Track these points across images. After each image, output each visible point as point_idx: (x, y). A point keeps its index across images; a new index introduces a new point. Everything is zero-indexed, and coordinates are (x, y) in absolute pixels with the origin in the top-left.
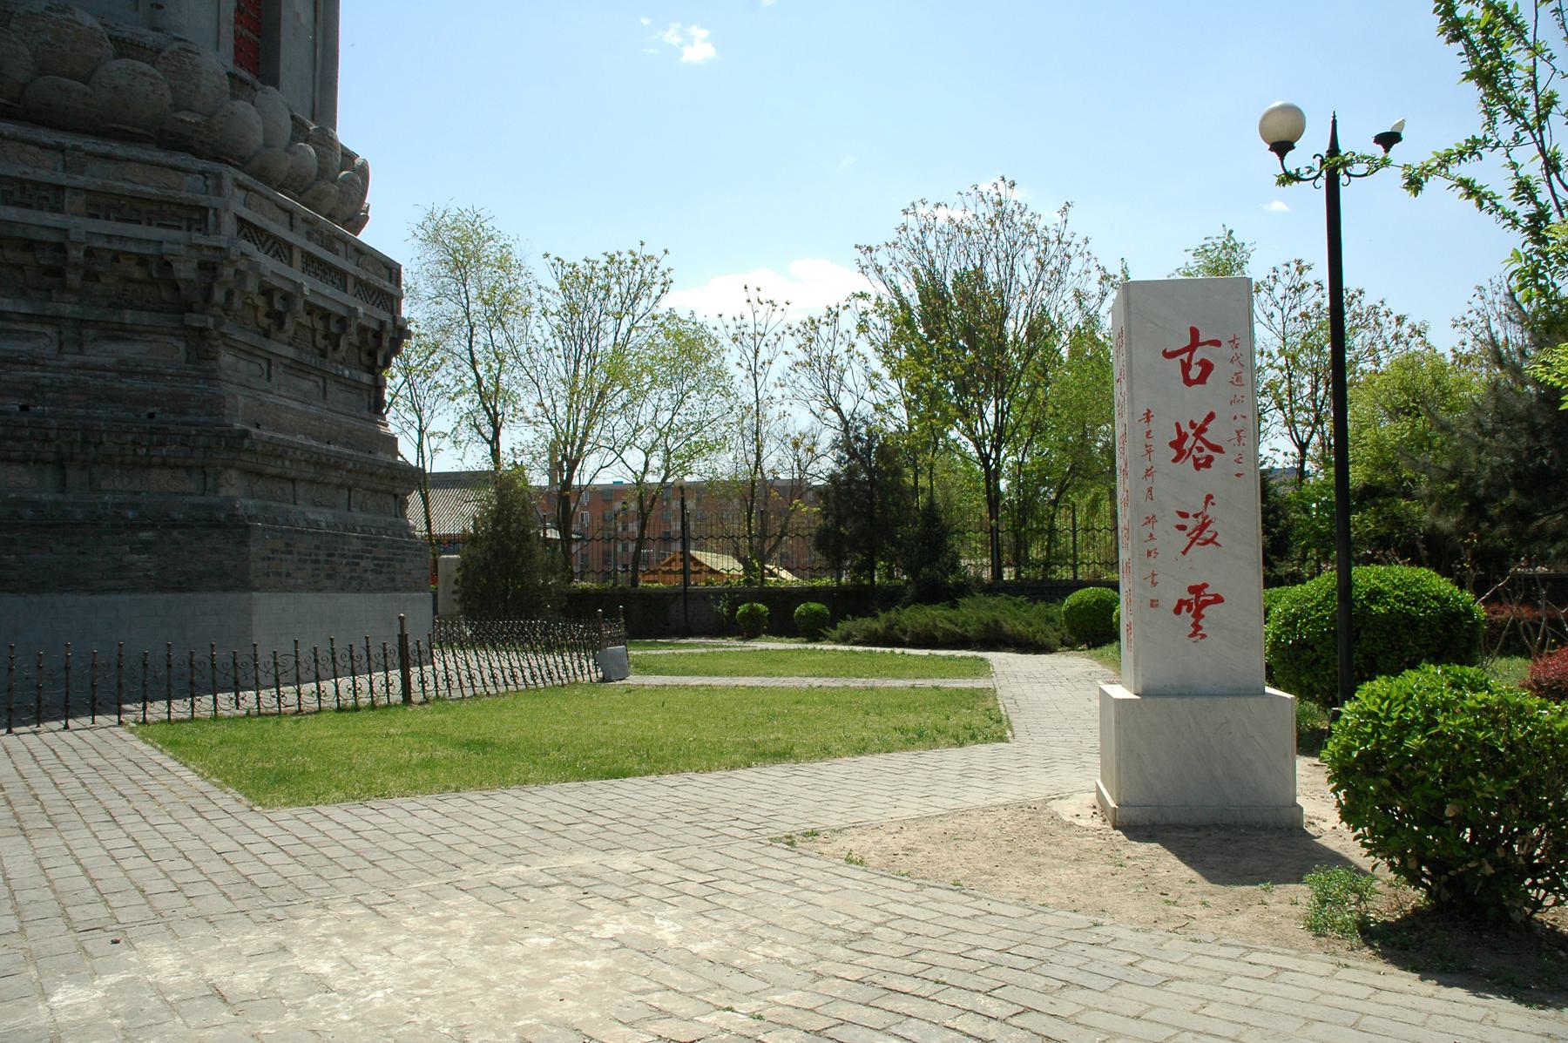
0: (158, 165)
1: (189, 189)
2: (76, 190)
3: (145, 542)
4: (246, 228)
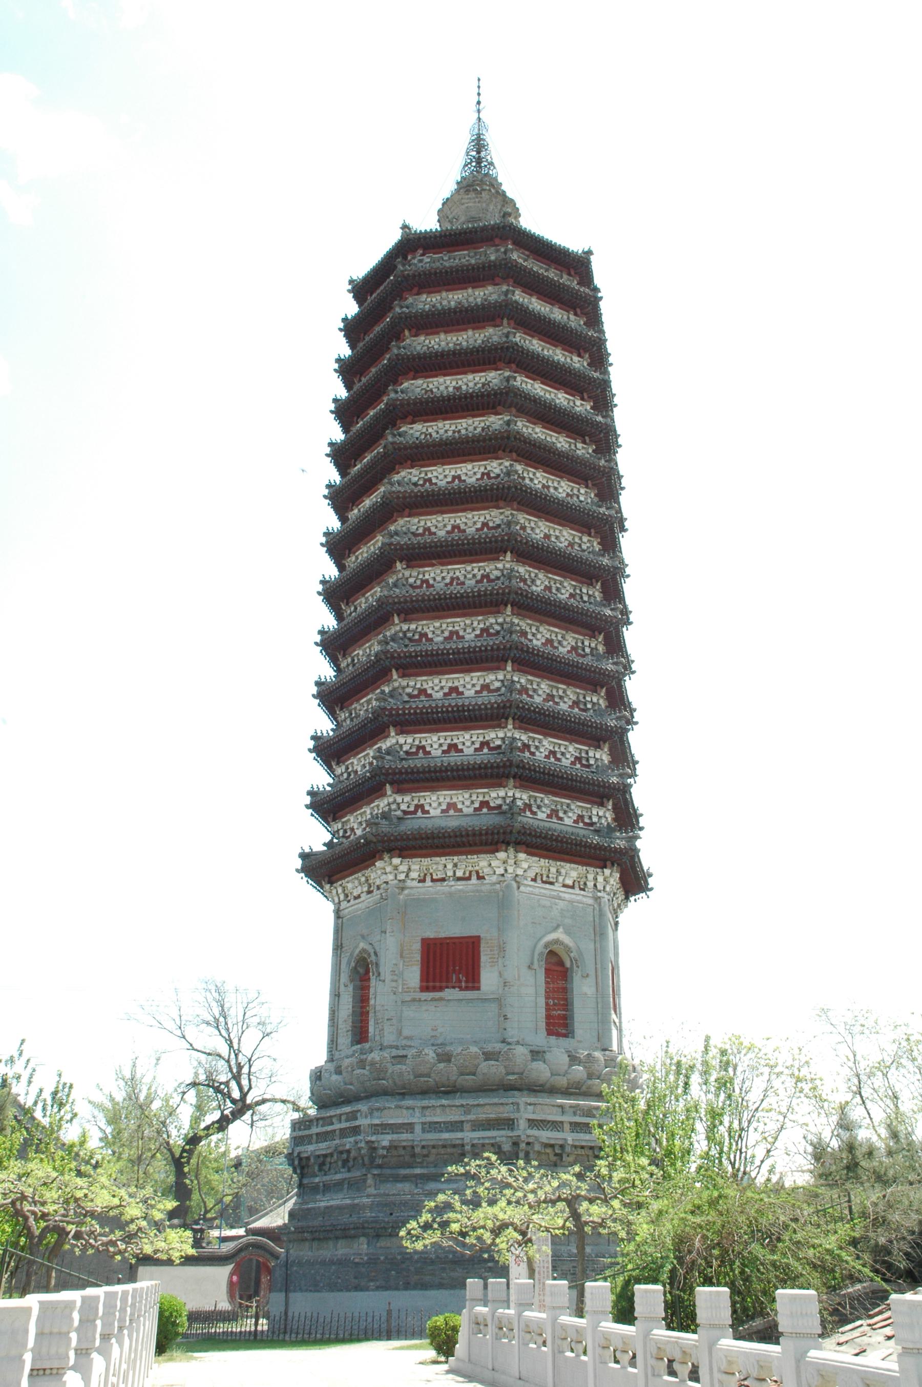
0: (496, 1104)
1: (506, 1112)
2: (467, 1121)
3: (490, 1268)
4: (533, 1123)
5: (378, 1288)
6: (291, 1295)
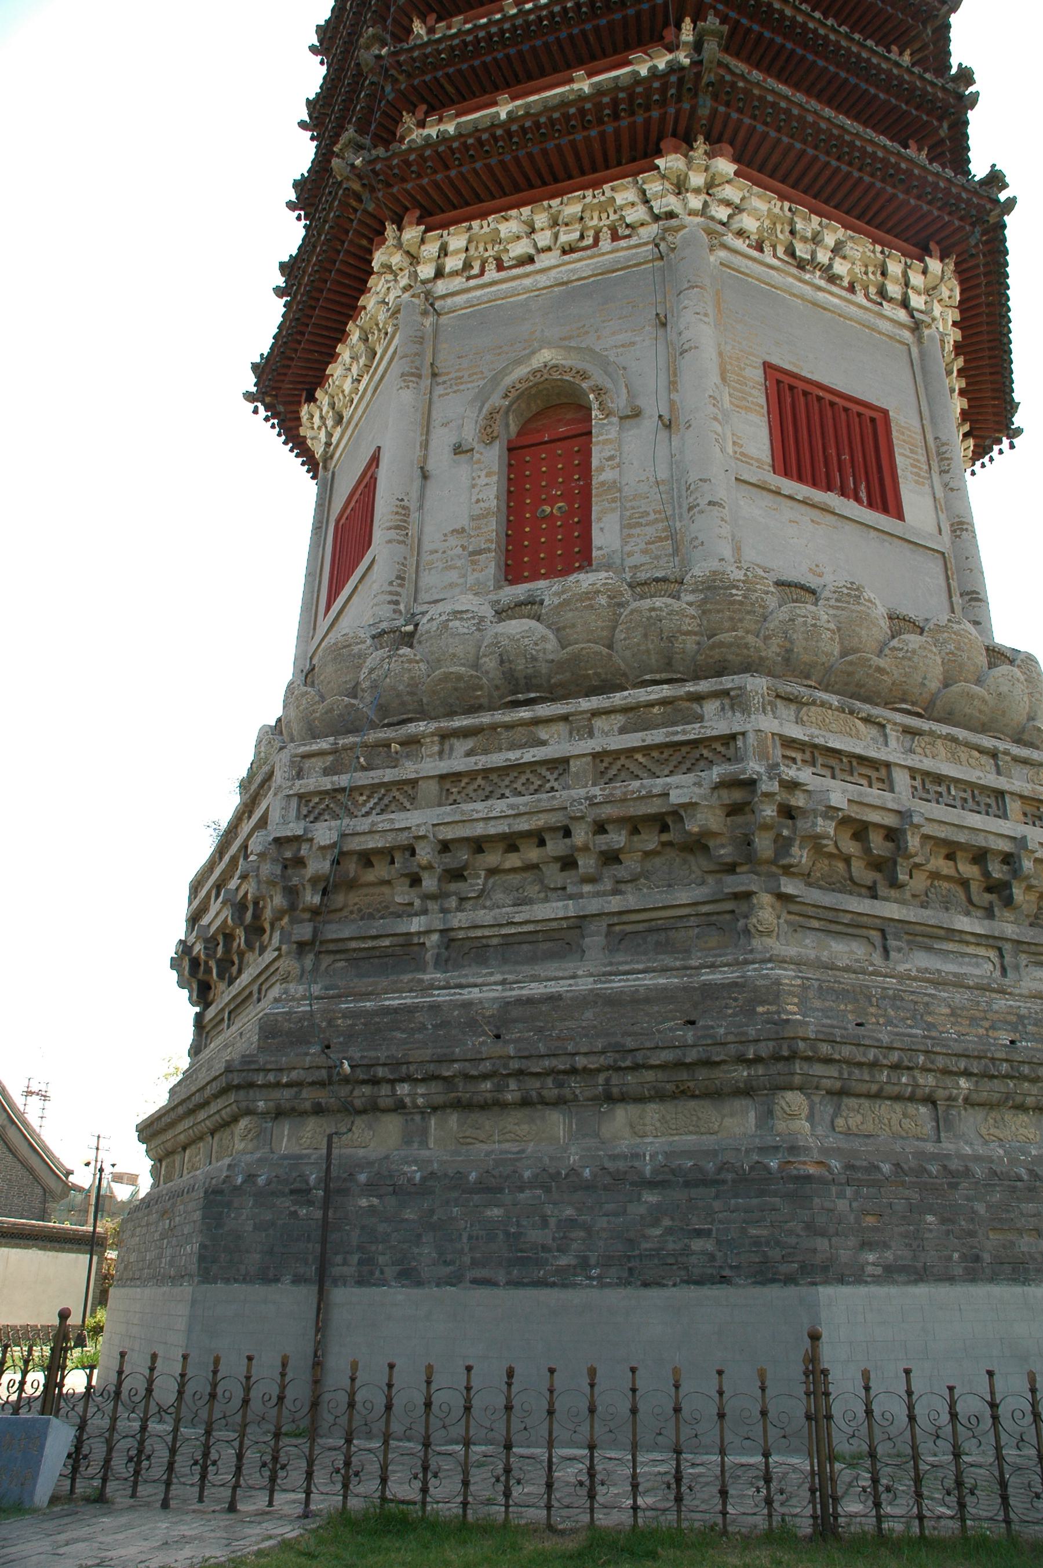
5: (890, 1274)
6: (345, 1298)
